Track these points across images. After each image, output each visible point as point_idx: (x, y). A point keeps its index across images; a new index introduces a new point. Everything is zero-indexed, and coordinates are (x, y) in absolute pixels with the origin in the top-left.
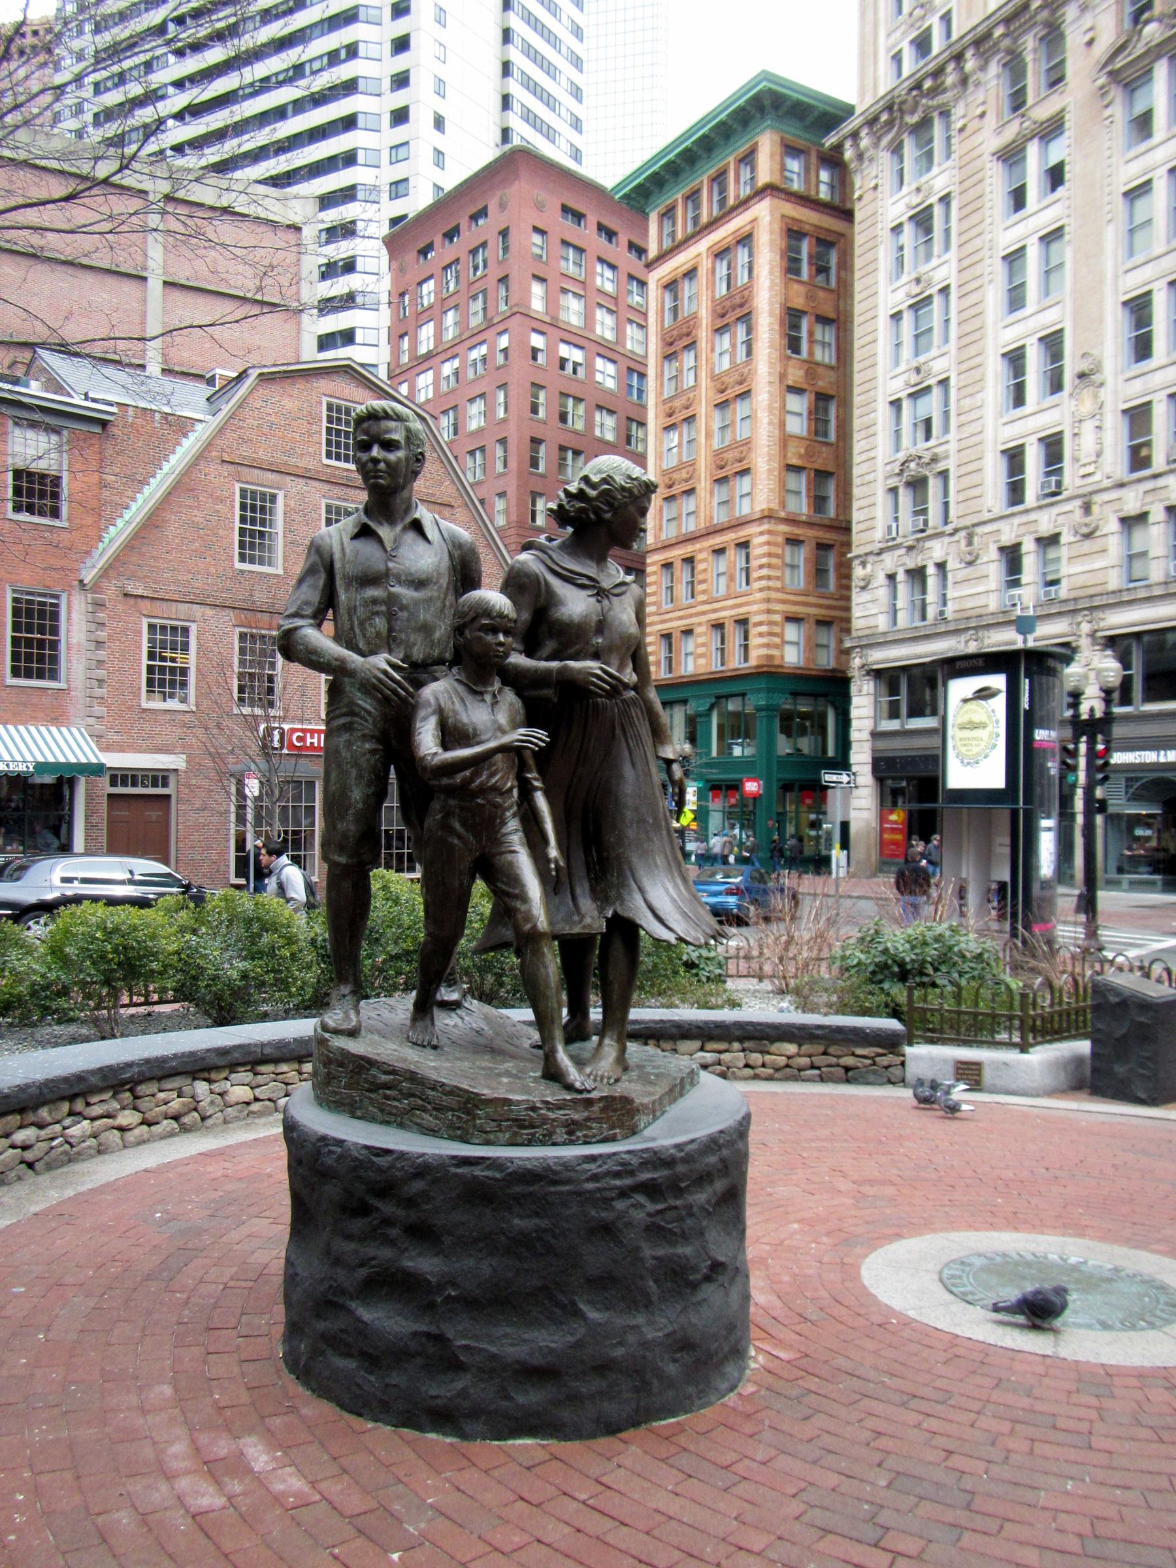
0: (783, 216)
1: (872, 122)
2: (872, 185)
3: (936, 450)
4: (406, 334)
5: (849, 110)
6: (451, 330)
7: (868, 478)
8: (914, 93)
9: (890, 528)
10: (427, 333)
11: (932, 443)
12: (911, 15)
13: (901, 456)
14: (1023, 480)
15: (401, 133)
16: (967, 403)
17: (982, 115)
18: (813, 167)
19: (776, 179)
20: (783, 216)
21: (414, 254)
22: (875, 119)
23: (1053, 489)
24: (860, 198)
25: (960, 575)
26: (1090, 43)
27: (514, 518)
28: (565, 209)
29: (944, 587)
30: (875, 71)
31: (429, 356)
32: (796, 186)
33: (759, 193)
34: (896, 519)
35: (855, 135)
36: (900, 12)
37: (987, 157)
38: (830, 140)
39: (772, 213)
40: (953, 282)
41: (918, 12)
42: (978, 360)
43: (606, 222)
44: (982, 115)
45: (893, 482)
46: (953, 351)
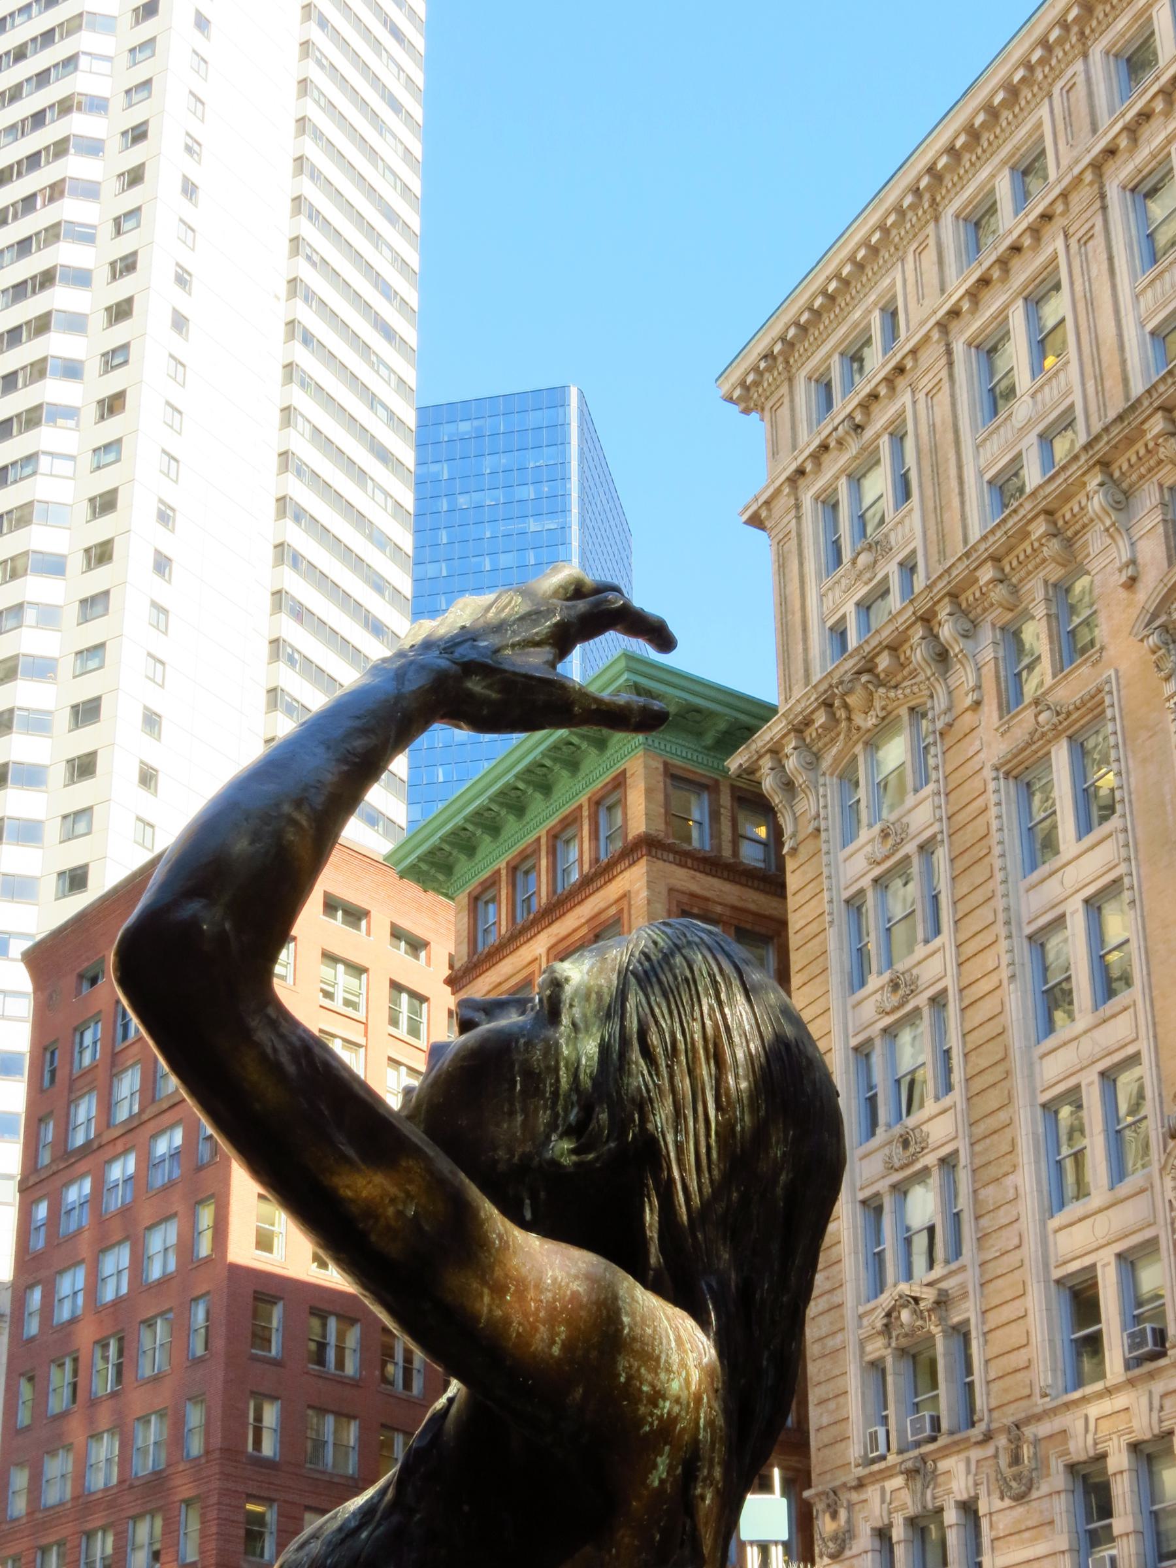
0: (671, 890)
1: (800, 728)
2: (810, 829)
3: (944, 1285)
4: (50, 1114)
5: (765, 712)
6: (125, 1105)
7: (831, 1343)
8: (864, 678)
9: (874, 1437)
10: (86, 1110)
11: (939, 1271)
12: (854, 562)
13: (886, 1300)
14: (1100, 1332)
15: (83, 794)
16: (989, 1194)
17: (978, 704)
18: (725, 813)
19: (659, 828)
20: (671, 890)
21: (72, 979)
22: (808, 722)
23: (1150, 1346)
24: (794, 850)
25: (1004, 1523)
26: (1132, 582)
27: (217, 1441)
28: (397, 934)
29: (978, 1549)
30: (806, 650)
31: (88, 1149)
32: (699, 840)
33: (631, 852)
34: (885, 1420)
35: (775, 751)
36: (839, 561)
37: (988, 773)
38: (735, 763)
39: (650, 884)
40: (949, 982)
41: (864, 559)
42: (1003, 1116)
43: (406, 924)
44: (978, 704)
45: (877, 1348)
46: (961, 1105)
